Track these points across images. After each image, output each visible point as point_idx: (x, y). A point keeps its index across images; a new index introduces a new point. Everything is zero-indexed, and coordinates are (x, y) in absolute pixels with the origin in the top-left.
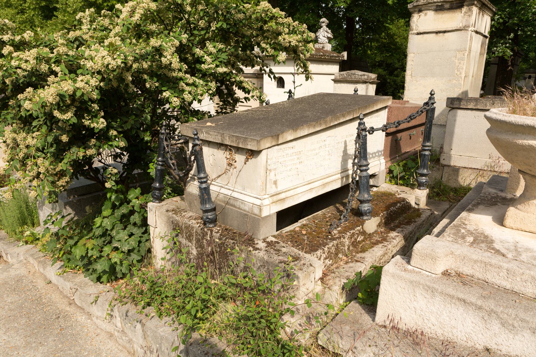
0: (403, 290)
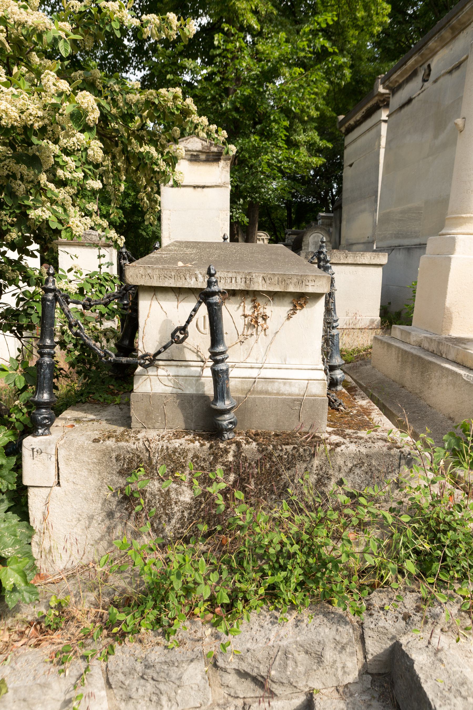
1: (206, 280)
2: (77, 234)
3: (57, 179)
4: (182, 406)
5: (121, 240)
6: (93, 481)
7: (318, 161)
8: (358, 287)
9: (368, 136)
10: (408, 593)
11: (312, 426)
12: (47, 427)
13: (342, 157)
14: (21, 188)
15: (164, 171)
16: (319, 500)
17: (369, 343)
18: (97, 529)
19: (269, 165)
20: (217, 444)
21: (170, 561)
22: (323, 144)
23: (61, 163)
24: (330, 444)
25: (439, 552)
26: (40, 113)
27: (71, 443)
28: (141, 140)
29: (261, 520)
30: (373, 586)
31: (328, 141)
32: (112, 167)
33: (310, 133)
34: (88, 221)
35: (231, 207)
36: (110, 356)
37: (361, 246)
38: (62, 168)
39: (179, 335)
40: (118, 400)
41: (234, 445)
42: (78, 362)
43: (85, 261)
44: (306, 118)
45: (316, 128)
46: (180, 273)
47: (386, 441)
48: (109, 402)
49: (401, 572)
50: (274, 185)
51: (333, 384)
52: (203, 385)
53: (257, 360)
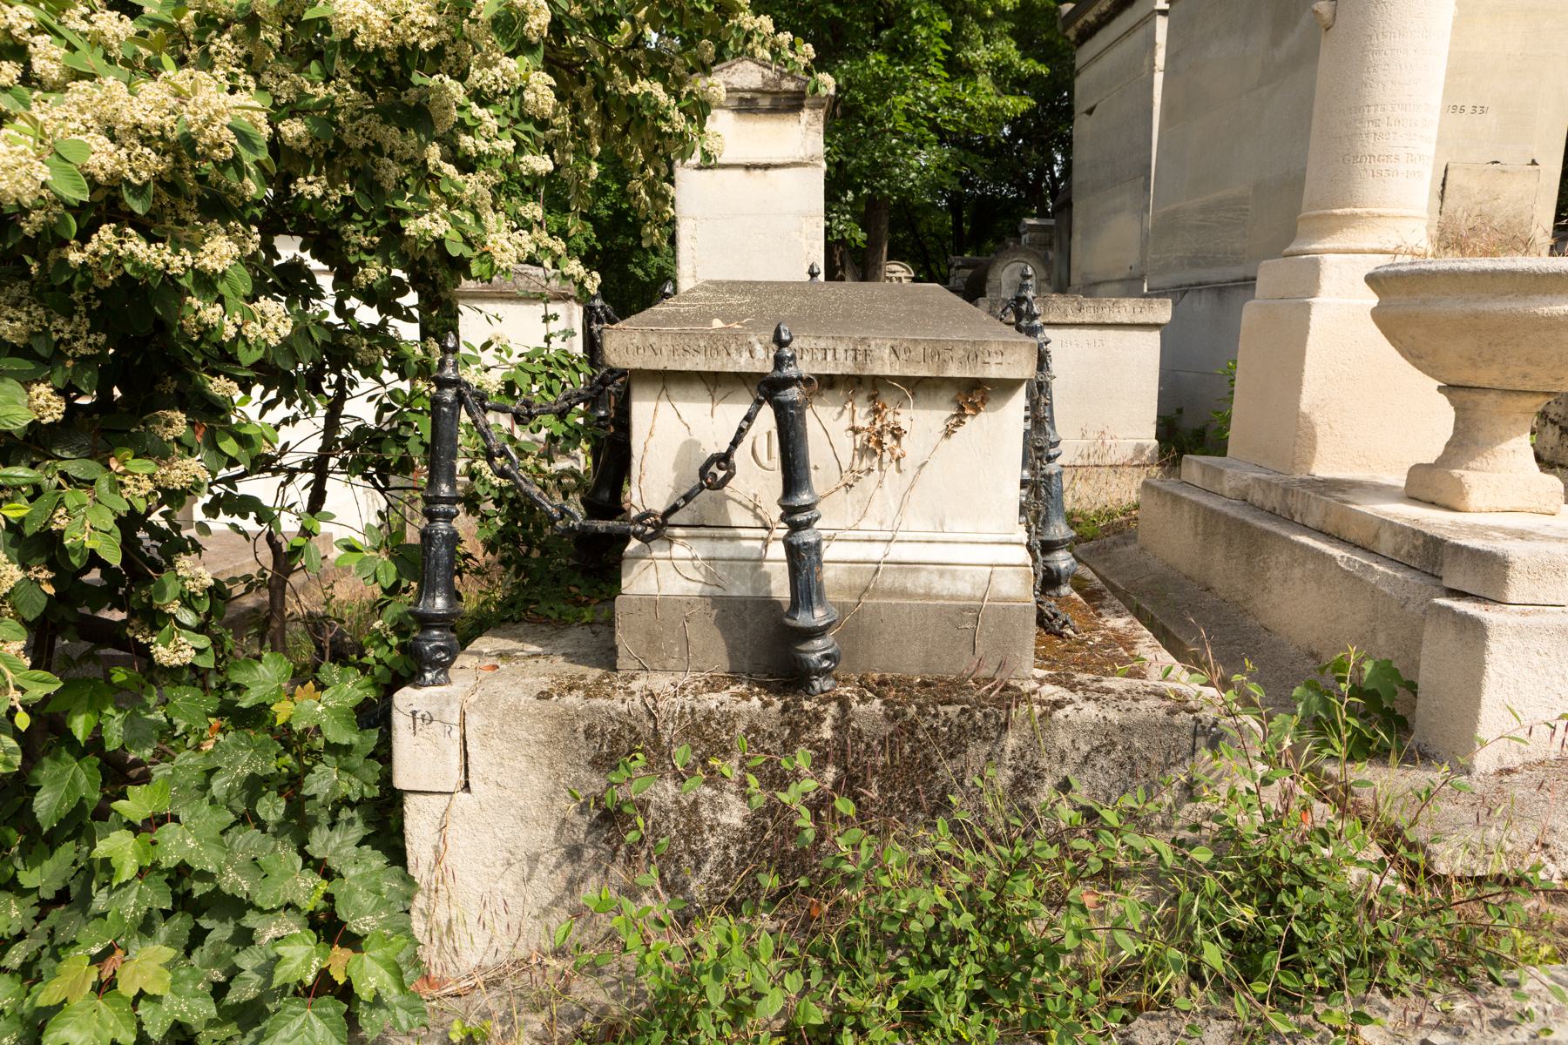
0: (1545, 658)
1: (771, 355)
2: (503, 266)
3: (460, 155)
4: (723, 623)
5: (593, 279)
6: (538, 781)
7: (1017, 104)
8: (1108, 375)
9: (1128, 45)
10: (1212, 1021)
11: (1001, 666)
12: (444, 667)
13: (1071, 93)
14: (391, 172)
15: (682, 133)
16: (1017, 822)
17: (1134, 497)
18: (546, 886)
19: (910, 116)
20: (797, 703)
21: (700, 949)
22: (1029, 66)
23: (469, 122)
24: (1041, 703)
25: (1278, 928)
26: (432, 21)
27: (492, 699)
28: (632, 69)
29: (893, 861)
30: (1135, 1008)
31: (1040, 62)
32: (572, 128)
33: (999, 45)
34: (524, 238)
35: (828, 209)
36: (573, 516)
37: (1117, 286)
38: (469, 131)
39: (716, 470)
40: (588, 615)
41: (834, 704)
42: (504, 540)
43: (507, 333)
44: (989, 12)
45: (1012, 33)
46: (717, 342)
47: (1163, 697)
48: (570, 619)
49: (1195, 974)
50: (923, 159)
51: (1049, 581)
52: (767, 577)
53: (881, 523)
